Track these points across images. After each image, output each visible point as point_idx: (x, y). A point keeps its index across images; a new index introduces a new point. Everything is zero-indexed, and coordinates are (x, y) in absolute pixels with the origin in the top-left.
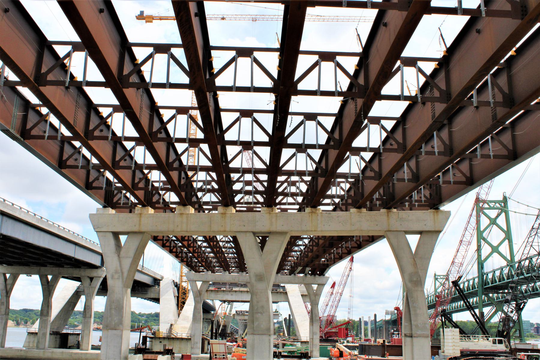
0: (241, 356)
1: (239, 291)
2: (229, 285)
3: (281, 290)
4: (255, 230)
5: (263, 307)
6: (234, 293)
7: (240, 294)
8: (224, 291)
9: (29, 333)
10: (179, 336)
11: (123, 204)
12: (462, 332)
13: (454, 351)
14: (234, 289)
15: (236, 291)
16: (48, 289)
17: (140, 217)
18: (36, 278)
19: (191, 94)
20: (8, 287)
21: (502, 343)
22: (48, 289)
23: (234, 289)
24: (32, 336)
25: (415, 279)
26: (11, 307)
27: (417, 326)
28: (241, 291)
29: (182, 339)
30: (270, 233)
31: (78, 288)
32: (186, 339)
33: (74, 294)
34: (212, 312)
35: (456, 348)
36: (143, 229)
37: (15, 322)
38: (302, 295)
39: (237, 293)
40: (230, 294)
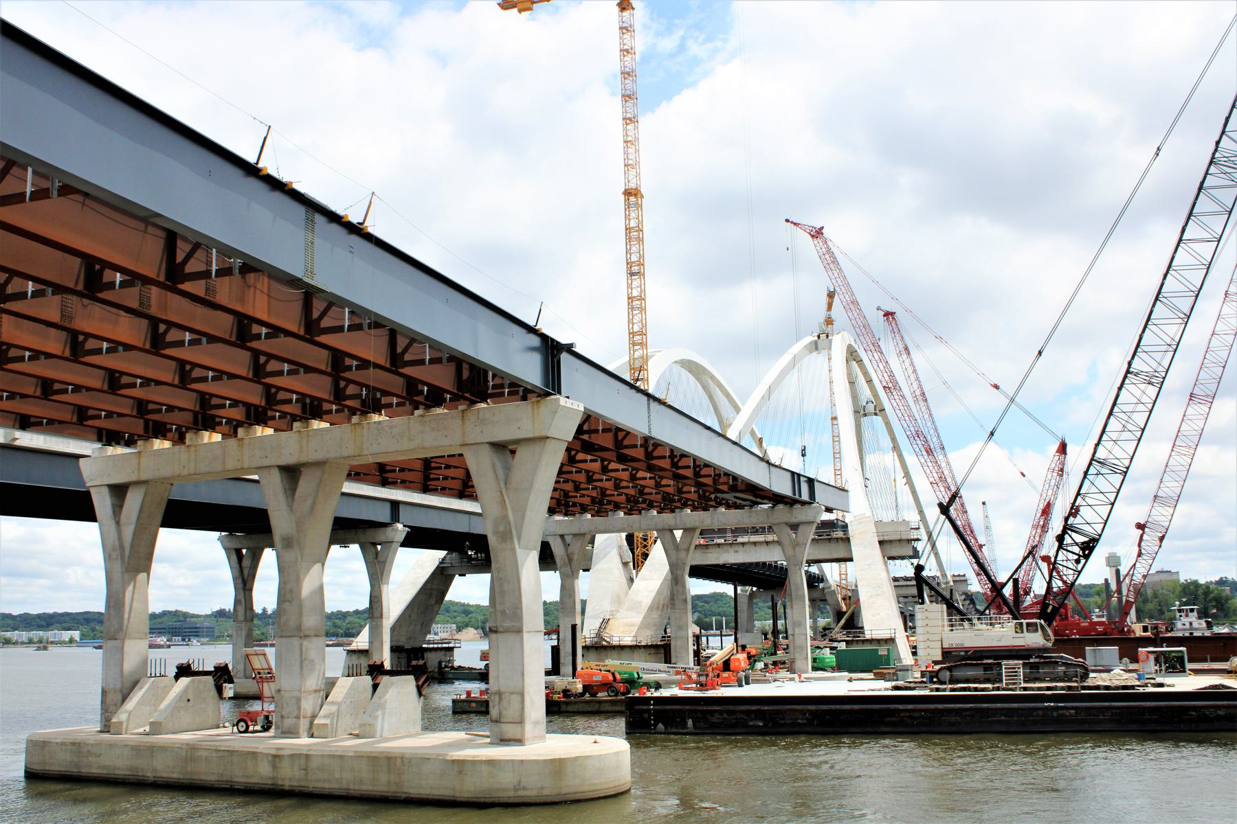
0: (592, 675)
1: (749, 543)
2: (733, 532)
3: (840, 534)
4: (283, 462)
5: (291, 591)
6: (740, 548)
7: (753, 547)
8: (719, 545)
9: (349, 651)
10: (615, 642)
11: (494, 387)
12: (951, 607)
13: (929, 651)
14: (740, 540)
15: (743, 544)
16: (378, 569)
17: (139, 457)
18: (355, 548)
19: (77, 267)
20: (246, 572)
21: (1036, 631)
22: (378, 569)
23: (740, 540)
24: (354, 657)
25: (502, 529)
26: (258, 609)
27: (503, 613)
28: (755, 543)
29: (622, 647)
30: (304, 465)
31: (443, 561)
32: (631, 647)
33: (433, 574)
34: (821, 585)
35: (932, 644)
36: (144, 477)
37: (480, 631)
38: (881, 543)
39: (746, 547)
40: (732, 550)
